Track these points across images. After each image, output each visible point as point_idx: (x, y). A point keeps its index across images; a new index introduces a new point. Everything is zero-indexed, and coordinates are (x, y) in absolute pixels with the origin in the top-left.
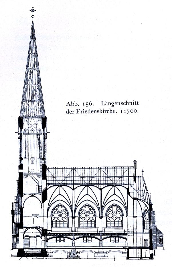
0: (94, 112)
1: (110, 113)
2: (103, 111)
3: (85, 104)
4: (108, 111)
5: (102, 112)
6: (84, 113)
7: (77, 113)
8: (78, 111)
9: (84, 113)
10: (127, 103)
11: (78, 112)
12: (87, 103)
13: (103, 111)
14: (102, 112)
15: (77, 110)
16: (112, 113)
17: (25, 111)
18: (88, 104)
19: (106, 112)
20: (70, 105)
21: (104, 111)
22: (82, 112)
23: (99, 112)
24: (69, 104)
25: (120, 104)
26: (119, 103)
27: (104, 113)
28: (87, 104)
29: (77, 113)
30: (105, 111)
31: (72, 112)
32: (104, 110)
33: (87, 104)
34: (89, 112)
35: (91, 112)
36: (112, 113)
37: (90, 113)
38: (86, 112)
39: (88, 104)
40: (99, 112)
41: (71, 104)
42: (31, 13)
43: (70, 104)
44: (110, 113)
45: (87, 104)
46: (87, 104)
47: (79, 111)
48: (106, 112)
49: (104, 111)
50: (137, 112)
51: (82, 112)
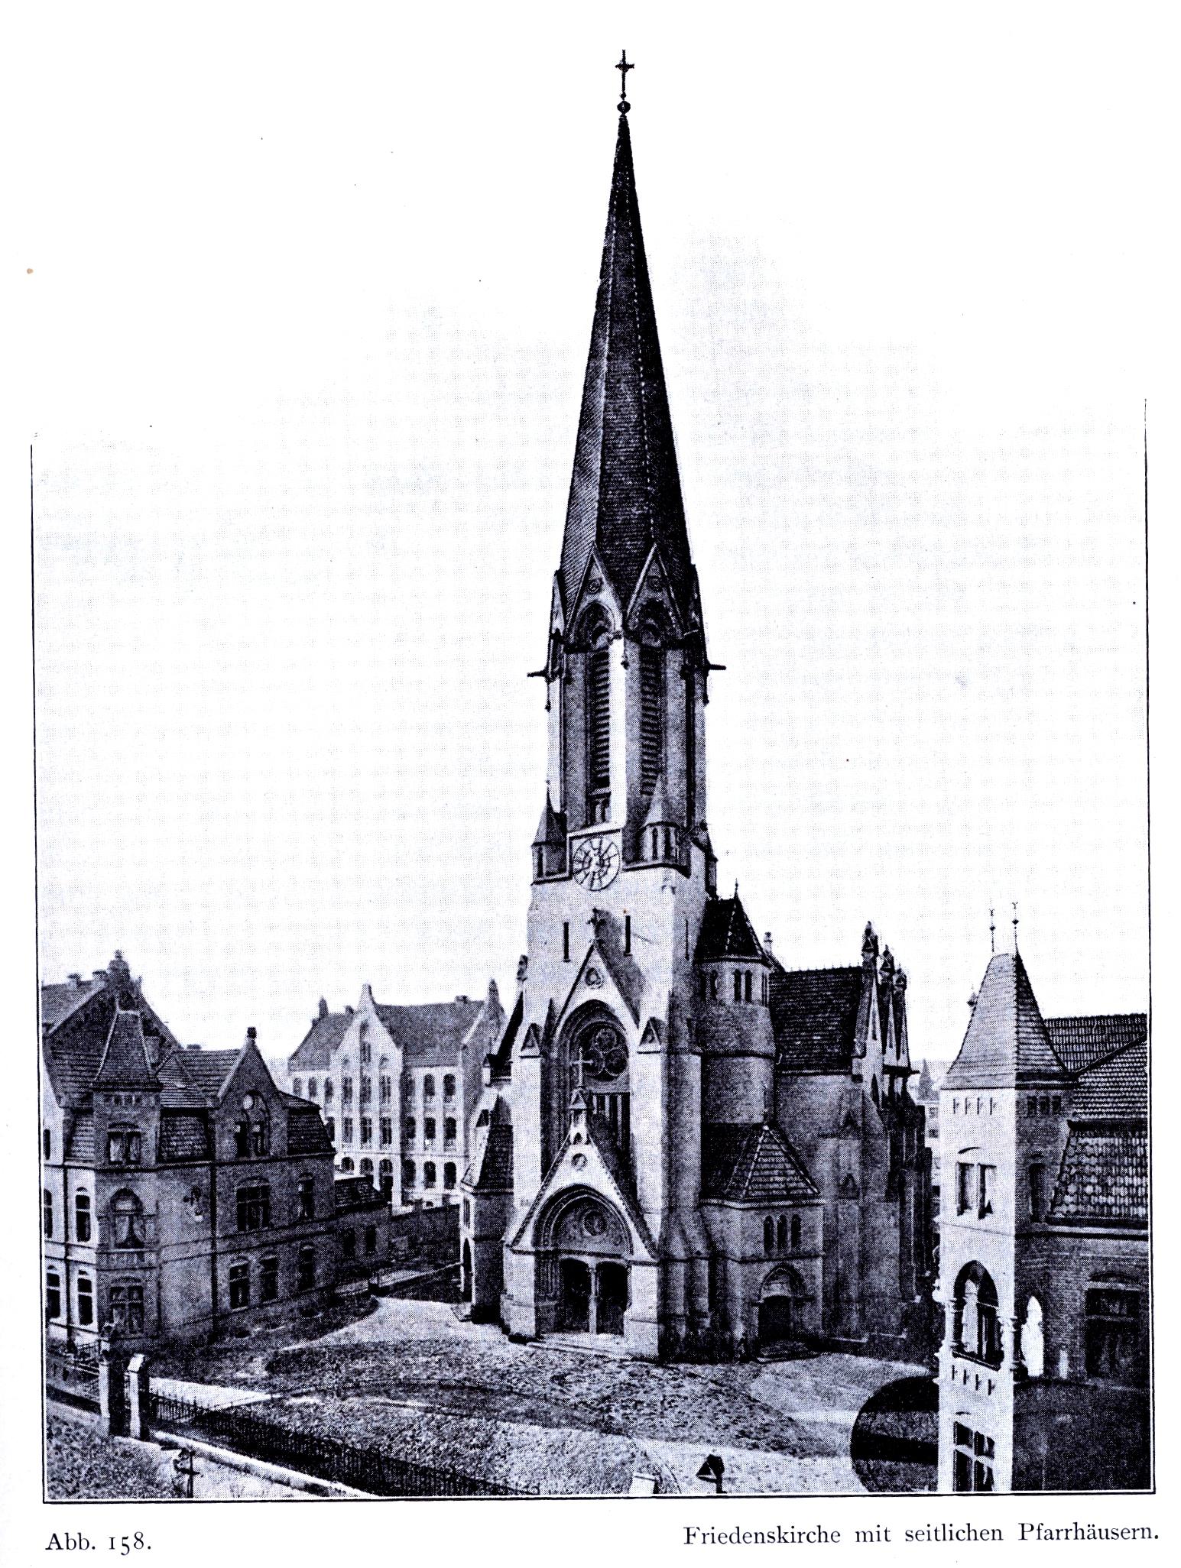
0: (1131, 1535)
1: (969, 1539)
2: (793, 1533)
3: (118, 1543)
4: (811, 1535)
5: (789, 1537)
6: (713, 1542)
7: (688, 1542)
8: (691, 1533)
9: (713, 1542)
10: (823, 1535)
11: (691, 1537)
12: (124, 1538)
13: (793, 1533)
14: (789, 1537)
15: (688, 1529)
16: (976, 1539)
17: (1029, 1057)
18: (131, 1542)
19: (804, 1537)
20: (60, 1548)
21: (797, 1537)
22: (709, 1538)
23: (776, 1536)
24: (57, 1542)
25: (766, 1538)
26: (760, 1537)
27: (797, 1544)
28: (124, 1545)
29: (688, 1542)
30: (800, 1534)
31: (1132, 1531)
32: (796, 1531)
33: (125, 1542)
34: (734, 1538)
35: (954, 1537)
36: (826, 1541)
37: (738, 1542)
38: (746, 1539)
39: (131, 1542)
40: (777, 1539)
41: (63, 1544)
42: (1013, 925)
43: (63, 1543)
44: (969, 1539)
45: (124, 1545)
46: (125, 1542)
47: (694, 1535)
48: (804, 1537)
49: (797, 1537)
50: (1036, 1528)
51: (709, 1538)
